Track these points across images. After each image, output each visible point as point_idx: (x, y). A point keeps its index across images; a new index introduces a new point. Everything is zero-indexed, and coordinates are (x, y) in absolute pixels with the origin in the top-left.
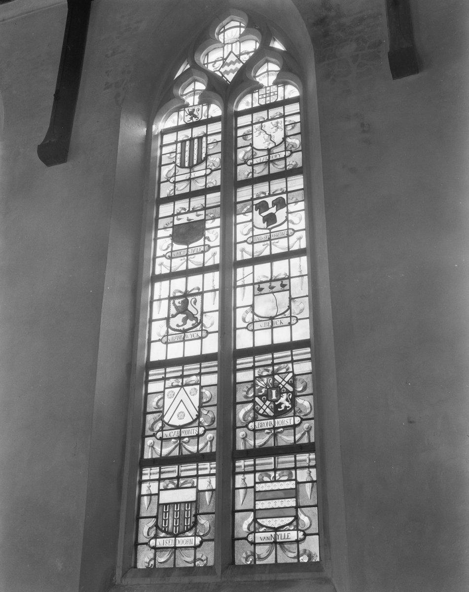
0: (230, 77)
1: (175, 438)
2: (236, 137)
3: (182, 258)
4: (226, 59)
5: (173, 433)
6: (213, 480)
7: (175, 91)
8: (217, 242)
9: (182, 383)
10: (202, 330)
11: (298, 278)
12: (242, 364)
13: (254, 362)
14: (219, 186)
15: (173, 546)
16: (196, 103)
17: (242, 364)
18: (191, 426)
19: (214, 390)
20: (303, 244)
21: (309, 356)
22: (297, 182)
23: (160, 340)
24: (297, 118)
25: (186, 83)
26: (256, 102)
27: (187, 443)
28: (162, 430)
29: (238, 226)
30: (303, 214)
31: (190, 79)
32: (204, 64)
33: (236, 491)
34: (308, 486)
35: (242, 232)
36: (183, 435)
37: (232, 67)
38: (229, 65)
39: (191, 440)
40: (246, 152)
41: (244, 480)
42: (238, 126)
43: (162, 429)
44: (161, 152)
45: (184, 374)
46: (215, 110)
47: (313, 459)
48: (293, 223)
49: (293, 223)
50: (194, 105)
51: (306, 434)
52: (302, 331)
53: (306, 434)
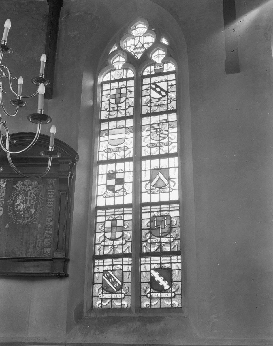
0: (139, 56)
1: (158, 243)
2: (142, 90)
3: (156, 148)
4: (136, 45)
5: (167, 240)
6: (130, 267)
7: (109, 60)
8: (132, 146)
9: (160, 214)
10: (124, 192)
11: (173, 169)
12: (118, 211)
13: (114, 212)
14: (132, 115)
15: (160, 297)
16: (120, 68)
17: (118, 211)
18: (119, 240)
19: (131, 222)
20: (176, 151)
21: (131, 212)
22: (173, 117)
23: (102, 195)
24: (174, 83)
25: (155, 50)
26: (112, 77)
27: (164, 245)
28: (151, 239)
29: (101, 143)
30: (132, 139)
31: (117, 55)
32: (125, 47)
33: (142, 273)
34: (177, 271)
35: (145, 141)
36: (162, 241)
37: (139, 50)
38: (137, 48)
39: (119, 247)
40: (106, 105)
41: (98, 269)
42: (143, 84)
43: (104, 241)
44: (102, 94)
45: (124, 213)
46: (131, 74)
47: (179, 259)
48: (171, 139)
49: (171, 139)
50: (119, 69)
51: (128, 249)
52: (175, 196)
53: (128, 249)
